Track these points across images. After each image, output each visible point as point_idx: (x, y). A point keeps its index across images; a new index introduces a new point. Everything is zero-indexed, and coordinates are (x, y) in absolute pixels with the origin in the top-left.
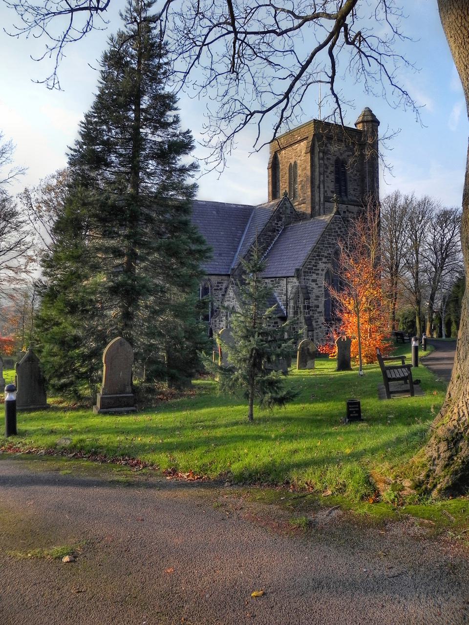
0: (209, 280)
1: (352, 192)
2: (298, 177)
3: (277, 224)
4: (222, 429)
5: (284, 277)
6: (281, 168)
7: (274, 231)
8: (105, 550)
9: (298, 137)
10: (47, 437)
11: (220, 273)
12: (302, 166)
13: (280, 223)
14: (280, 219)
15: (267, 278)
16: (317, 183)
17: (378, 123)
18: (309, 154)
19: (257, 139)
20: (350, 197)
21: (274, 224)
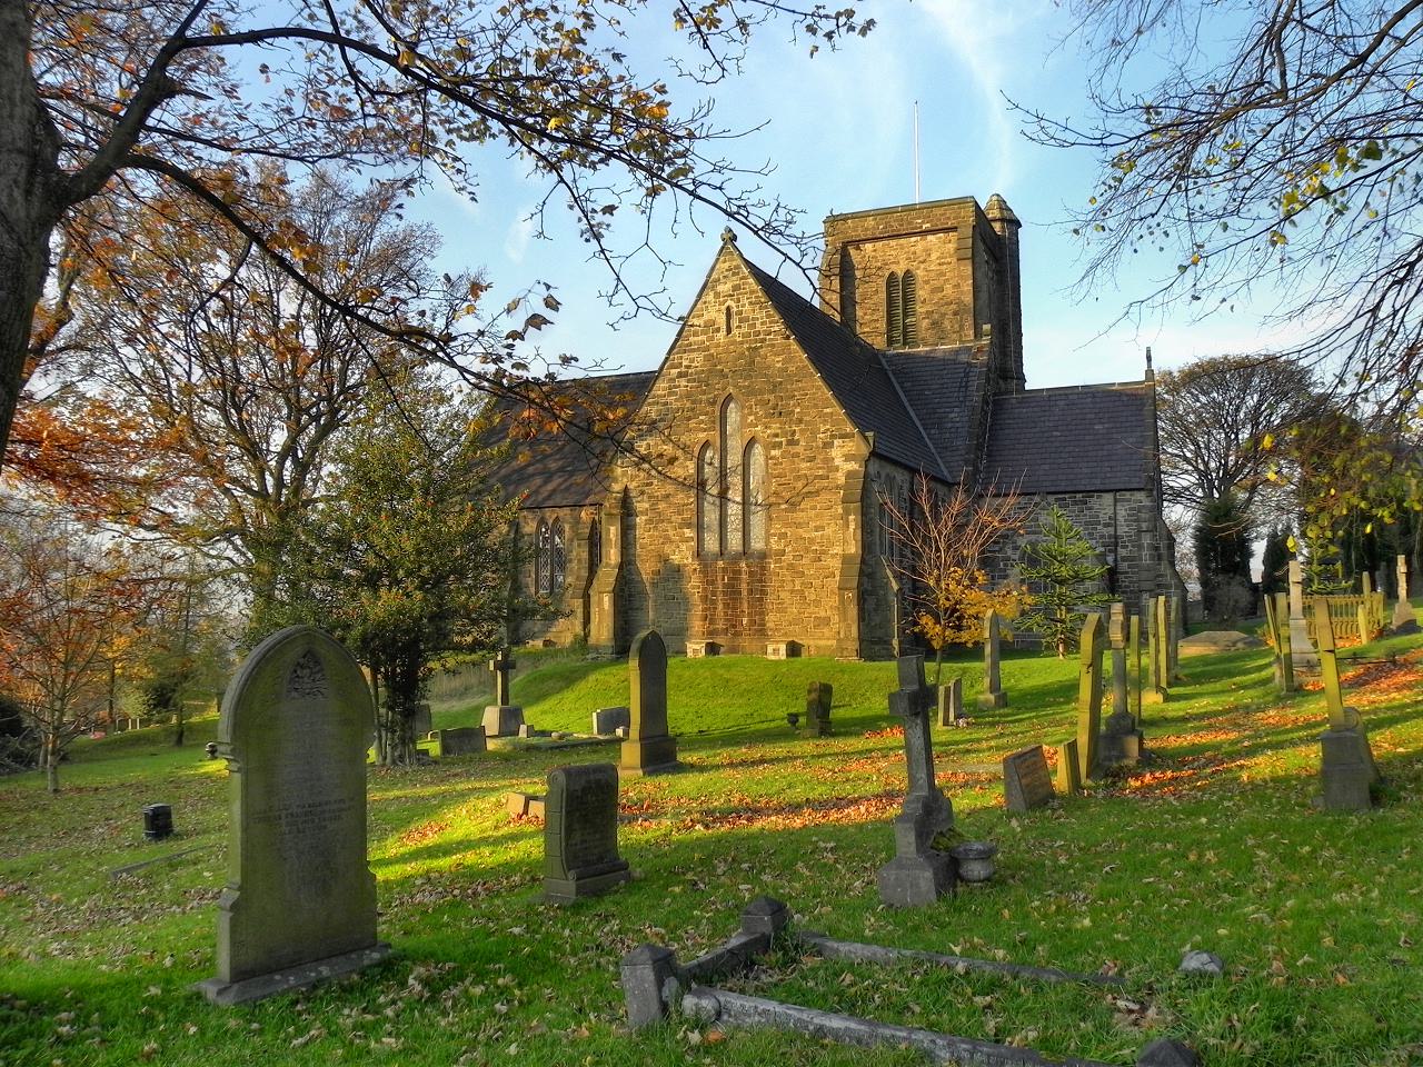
17: (1019, 225)
18: (969, 262)
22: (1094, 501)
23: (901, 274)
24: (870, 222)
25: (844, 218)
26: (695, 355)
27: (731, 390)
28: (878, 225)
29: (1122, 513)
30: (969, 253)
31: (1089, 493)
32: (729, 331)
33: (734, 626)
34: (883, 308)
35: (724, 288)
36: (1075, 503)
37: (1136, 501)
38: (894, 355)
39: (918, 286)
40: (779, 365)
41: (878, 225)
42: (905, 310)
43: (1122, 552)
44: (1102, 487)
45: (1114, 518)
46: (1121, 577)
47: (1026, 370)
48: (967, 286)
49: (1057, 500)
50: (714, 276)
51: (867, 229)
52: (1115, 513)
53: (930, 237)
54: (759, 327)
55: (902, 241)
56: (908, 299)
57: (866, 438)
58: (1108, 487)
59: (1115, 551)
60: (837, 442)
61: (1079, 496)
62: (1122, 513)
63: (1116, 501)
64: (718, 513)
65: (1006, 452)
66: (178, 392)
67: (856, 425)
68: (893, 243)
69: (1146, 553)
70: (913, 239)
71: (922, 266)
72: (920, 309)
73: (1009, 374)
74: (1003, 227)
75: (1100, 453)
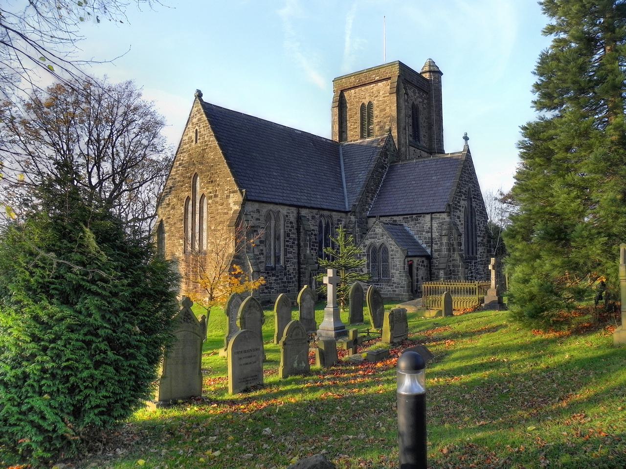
0: (331, 217)
1: (423, 138)
2: (375, 118)
3: (385, 161)
4: (458, 352)
5: (428, 214)
6: (349, 107)
7: (383, 168)
8: (548, 373)
9: (376, 77)
10: (274, 359)
11: (340, 209)
12: (380, 107)
13: (387, 160)
14: (386, 156)
15: (398, 215)
16: (403, 125)
17: (442, 74)
18: (395, 95)
19: (29, 57)
20: (421, 143)
21: (382, 161)
22: (421, 219)
23: (366, 104)
24: (353, 79)
25: (341, 78)
26: (185, 154)
27: (196, 171)
28: (356, 80)
29: (435, 225)
30: (395, 90)
31: (419, 215)
32: (196, 142)
33: (195, 288)
34: (359, 121)
35: (195, 120)
36: (412, 220)
37: (442, 219)
38: (346, 145)
39: (374, 109)
40: (212, 157)
41: (356, 80)
42: (369, 121)
43: (435, 247)
44: (425, 211)
45: (431, 228)
46: (435, 261)
47: (445, 149)
48: (394, 108)
49: (404, 218)
50: (192, 115)
51: (351, 83)
52: (431, 226)
53: (379, 84)
54: (206, 139)
55: (367, 87)
56: (370, 116)
57: (242, 193)
58: (428, 211)
59: (432, 246)
60: (232, 195)
61: (414, 216)
62: (435, 225)
63: (432, 219)
64: (371, 219)
65: (386, 194)
66: (386, 168)
67: (239, 185)
68: (363, 88)
69: (444, 248)
70: (372, 85)
71: (376, 98)
72: (375, 120)
73: (433, 151)
74: (430, 75)
75: (431, 192)
